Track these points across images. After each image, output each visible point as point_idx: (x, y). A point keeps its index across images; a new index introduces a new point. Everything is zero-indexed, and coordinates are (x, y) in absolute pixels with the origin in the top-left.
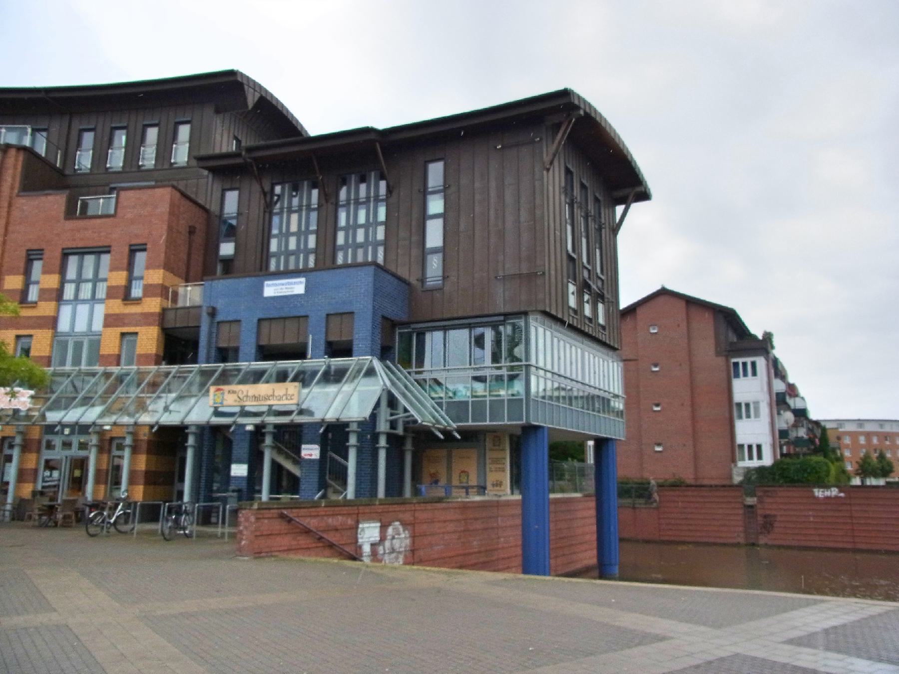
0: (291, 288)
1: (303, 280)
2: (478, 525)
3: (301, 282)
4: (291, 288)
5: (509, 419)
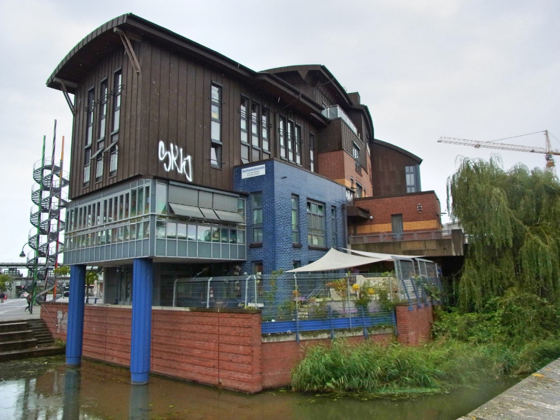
0: (257, 172)
1: (264, 165)
2: (96, 320)
3: (263, 168)
4: (257, 172)
5: (178, 256)
